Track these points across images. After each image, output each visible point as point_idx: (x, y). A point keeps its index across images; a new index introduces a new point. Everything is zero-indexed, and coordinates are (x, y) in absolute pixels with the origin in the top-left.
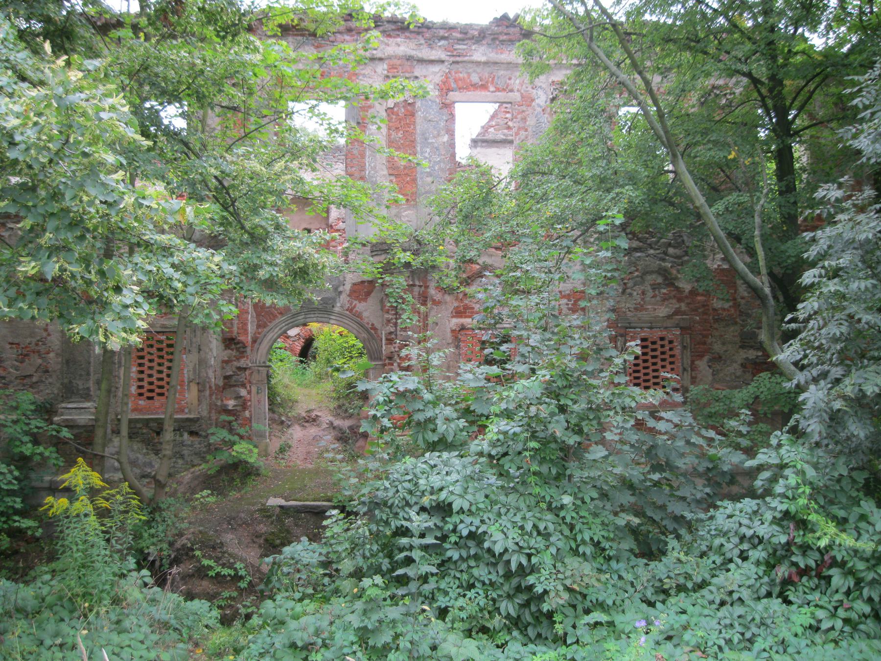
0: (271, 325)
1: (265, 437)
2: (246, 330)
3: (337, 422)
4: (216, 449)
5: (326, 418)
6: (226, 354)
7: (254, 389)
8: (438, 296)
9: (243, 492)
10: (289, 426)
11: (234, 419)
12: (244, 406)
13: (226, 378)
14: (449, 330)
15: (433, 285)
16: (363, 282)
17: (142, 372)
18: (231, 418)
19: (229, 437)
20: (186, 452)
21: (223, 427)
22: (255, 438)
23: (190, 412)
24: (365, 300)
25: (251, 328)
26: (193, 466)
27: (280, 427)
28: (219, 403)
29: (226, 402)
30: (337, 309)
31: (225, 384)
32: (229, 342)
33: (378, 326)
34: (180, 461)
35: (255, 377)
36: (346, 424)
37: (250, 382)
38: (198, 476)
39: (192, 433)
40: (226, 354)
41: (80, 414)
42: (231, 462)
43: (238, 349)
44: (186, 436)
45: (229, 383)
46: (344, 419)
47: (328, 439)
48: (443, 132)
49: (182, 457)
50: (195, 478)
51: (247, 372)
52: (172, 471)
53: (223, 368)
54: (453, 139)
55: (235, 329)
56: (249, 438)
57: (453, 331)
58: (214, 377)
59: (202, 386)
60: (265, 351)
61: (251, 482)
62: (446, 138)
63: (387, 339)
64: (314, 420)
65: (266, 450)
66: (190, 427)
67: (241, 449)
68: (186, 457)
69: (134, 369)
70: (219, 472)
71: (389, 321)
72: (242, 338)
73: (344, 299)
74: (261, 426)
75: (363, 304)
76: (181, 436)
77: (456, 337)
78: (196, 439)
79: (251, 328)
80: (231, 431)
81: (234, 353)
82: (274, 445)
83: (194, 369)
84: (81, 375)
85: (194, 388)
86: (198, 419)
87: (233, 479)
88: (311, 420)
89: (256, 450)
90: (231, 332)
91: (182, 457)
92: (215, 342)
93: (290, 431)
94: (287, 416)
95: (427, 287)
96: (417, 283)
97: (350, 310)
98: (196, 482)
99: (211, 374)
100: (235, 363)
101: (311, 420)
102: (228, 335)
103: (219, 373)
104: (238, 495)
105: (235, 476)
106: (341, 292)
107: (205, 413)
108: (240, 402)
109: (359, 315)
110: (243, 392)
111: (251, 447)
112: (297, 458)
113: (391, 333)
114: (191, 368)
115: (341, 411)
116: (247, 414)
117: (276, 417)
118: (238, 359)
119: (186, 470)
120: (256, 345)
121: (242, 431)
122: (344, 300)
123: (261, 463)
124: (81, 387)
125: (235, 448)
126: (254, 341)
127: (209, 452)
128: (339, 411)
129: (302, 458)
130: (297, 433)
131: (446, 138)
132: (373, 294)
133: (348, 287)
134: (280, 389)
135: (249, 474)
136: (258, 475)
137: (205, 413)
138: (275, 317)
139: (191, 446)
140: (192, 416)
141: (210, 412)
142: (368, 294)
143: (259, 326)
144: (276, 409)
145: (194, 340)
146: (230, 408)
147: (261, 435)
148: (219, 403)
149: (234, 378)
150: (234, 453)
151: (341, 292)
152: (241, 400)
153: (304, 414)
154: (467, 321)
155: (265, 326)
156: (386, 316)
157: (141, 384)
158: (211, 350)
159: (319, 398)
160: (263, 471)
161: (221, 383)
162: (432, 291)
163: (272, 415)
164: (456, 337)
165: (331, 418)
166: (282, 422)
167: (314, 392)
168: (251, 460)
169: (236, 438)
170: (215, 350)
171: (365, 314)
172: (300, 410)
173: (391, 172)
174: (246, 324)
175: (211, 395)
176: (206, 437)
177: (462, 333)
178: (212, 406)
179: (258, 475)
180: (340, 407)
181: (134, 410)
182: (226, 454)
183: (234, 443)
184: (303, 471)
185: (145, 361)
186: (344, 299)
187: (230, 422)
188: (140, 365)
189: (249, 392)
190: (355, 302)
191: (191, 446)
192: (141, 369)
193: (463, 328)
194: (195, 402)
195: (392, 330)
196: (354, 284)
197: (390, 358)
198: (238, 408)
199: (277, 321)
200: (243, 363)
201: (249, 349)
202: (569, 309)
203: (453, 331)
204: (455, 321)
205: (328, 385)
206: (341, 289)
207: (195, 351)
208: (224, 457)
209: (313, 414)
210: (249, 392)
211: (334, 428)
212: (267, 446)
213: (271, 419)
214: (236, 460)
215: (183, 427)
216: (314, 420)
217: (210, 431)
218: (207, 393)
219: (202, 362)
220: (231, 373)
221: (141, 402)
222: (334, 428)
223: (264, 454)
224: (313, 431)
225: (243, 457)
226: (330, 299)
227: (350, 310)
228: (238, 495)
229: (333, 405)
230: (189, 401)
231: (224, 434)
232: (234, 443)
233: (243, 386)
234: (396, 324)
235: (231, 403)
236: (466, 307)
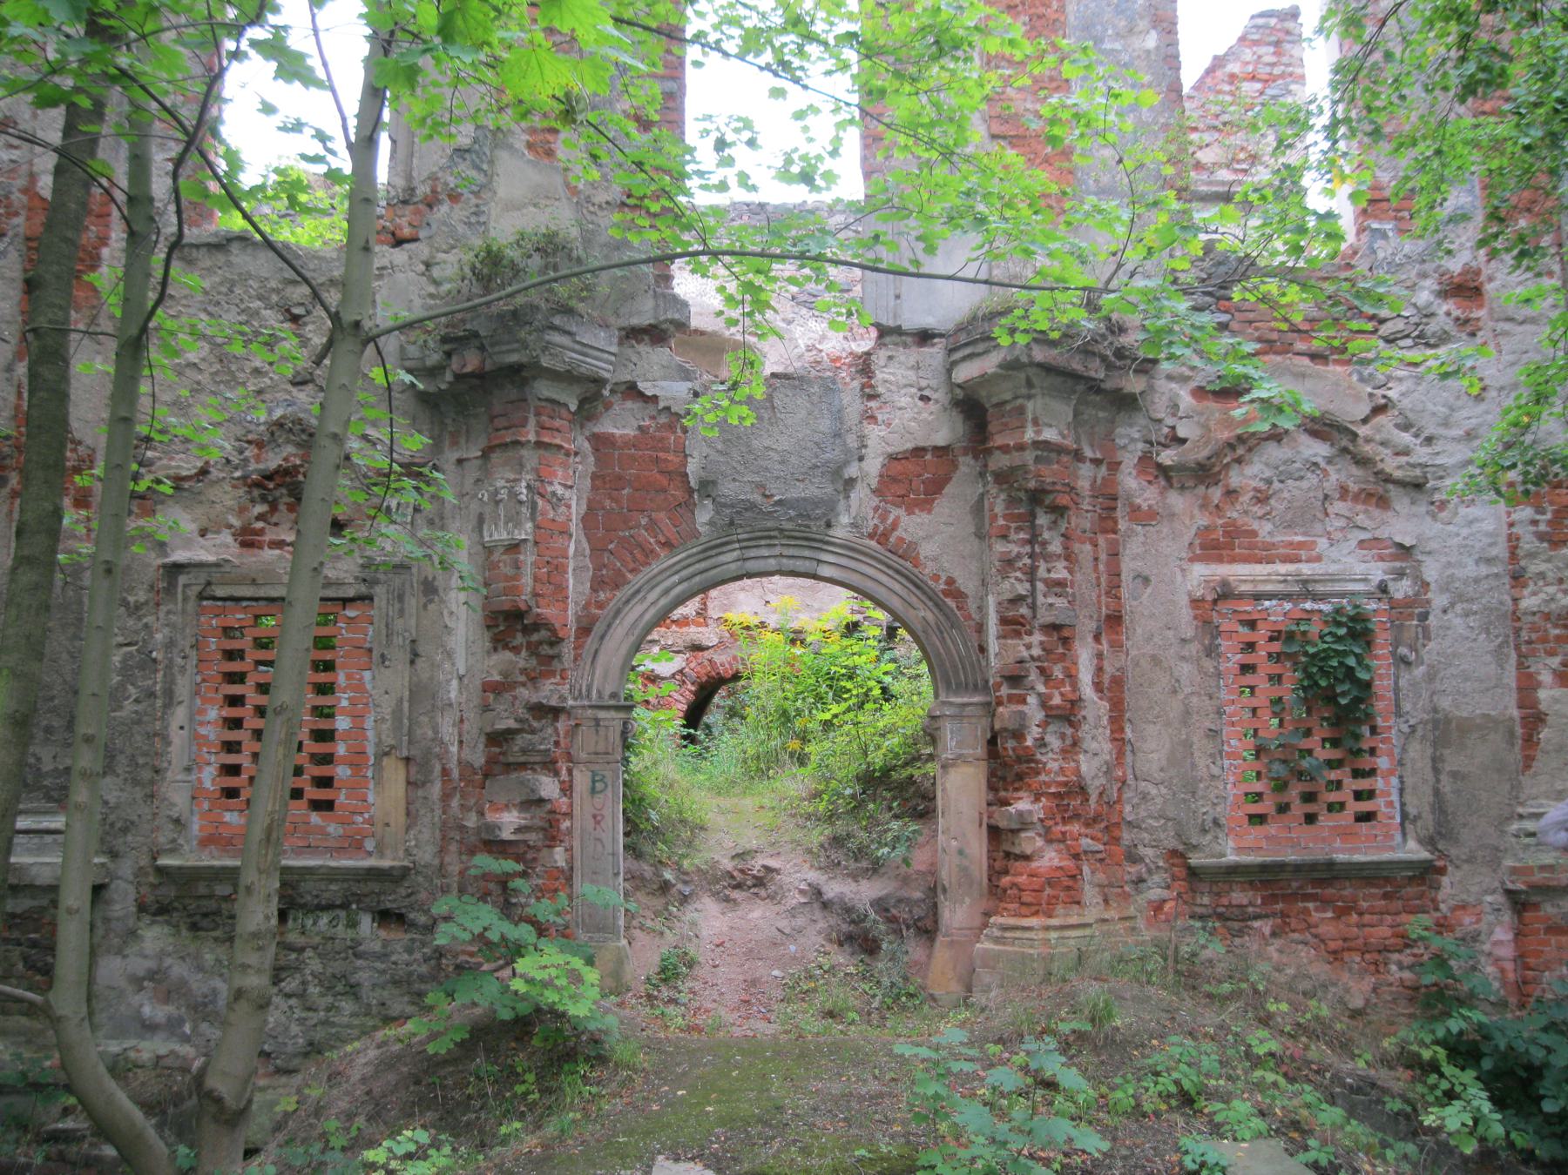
0: (637, 580)
1: (614, 930)
2: (561, 589)
3: (834, 888)
4: (459, 968)
5: (797, 874)
6: (496, 665)
7: (581, 779)
8: (1145, 494)
9: (551, 1130)
10: (684, 899)
11: (516, 871)
12: (551, 833)
13: (497, 739)
14: (1184, 601)
15: (1129, 460)
16: (918, 451)
17: (236, 723)
18: (510, 866)
19: (500, 928)
20: (364, 977)
21: (483, 898)
22: (582, 936)
23: (380, 851)
24: (926, 504)
25: (576, 586)
26: (388, 1020)
27: (658, 903)
28: (471, 821)
29: (491, 817)
30: (840, 532)
31: (491, 761)
32: (509, 624)
33: (968, 585)
34: (347, 1006)
35: (585, 743)
36: (863, 893)
37: (569, 757)
38: (399, 1057)
39: (385, 917)
40: (496, 665)
41: (40, 850)
42: (506, 1015)
43: (533, 649)
44: (366, 923)
45: (503, 755)
46: (855, 877)
47: (813, 940)
48: (1143, 24)
49: (353, 990)
50: (387, 1064)
51: (562, 725)
52: (319, 1035)
53: (486, 708)
54: (1174, 44)
55: (527, 581)
56: (565, 933)
57: (1196, 603)
58: (456, 737)
59: (417, 767)
60: (617, 662)
61: (575, 1086)
62: (1151, 41)
63: (1004, 621)
64: (760, 882)
65: (617, 974)
66: (386, 898)
67: (543, 971)
68: (365, 992)
69: (213, 714)
70: (466, 1048)
71: (1009, 562)
72: (548, 611)
73: (861, 501)
74: (604, 892)
75: (921, 517)
76: (353, 924)
77: (1207, 623)
78: (398, 937)
79: (576, 586)
80: (508, 909)
81: (522, 660)
82: (644, 957)
83: (397, 712)
84: (49, 730)
85: (396, 776)
86: (405, 873)
87: (513, 1076)
88: (748, 882)
89: (592, 975)
90: (515, 590)
91: (353, 990)
92: (462, 611)
93: (689, 914)
94: (680, 870)
95: (1115, 466)
96: (1088, 453)
97: (882, 537)
98: (392, 1077)
99: (448, 731)
100: (524, 693)
101: (748, 882)
102: (505, 603)
103: (473, 726)
104: (531, 1142)
105: (520, 1061)
106: (850, 483)
107: (426, 855)
108: (538, 817)
109: (907, 552)
110: (548, 787)
111: (577, 963)
112: (717, 997)
113: (1017, 600)
114: (387, 711)
115: (844, 852)
116: (559, 856)
117: (647, 870)
118: (533, 679)
119: (365, 1032)
120: (590, 642)
121: (544, 910)
122: (858, 509)
123: (611, 1021)
124: (47, 766)
125: (522, 965)
126: (584, 630)
127: (434, 977)
128: (835, 855)
129: (733, 998)
130: (709, 920)
131: (1151, 41)
132: (948, 489)
133: (873, 465)
134: (652, 789)
135: (570, 1056)
136: (602, 1060)
137: (426, 855)
138: (649, 554)
139: (382, 957)
140: (386, 863)
141: (442, 851)
142: (936, 487)
143: (598, 584)
144: (647, 848)
145: (399, 624)
146: (506, 835)
147: (602, 926)
148: (471, 821)
149: (521, 741)
150: (518, 985)
151: (850, 483)
152: (540, 813)
153: (727, 864)
154: (1241, 573)
155: (617, 583)
156: (1000, 547)
157: (232, 759)
158: (449, 655)
159: (766, 818)
160: (621, 1052)
161: (478, 758)
162: (1130, 481)
163: (635, 865)
164: (1207, 623)
165: (813, 876)
166: (665, 887)
167: (749, 803)
168: (578, 1010)
169: (525, 932)
170: (461, 645)
171: (926, 550)
172: (717, 851)
173: (997, 128)
174: (560, 569)
175: (446, 797)
176: (430, 928)
177: (1224, 607)
178: (449, 832)
179: (602, 1060)
180: (837, 841)
181: (205, 842)
182: (491, 988)
183: (516, 950)
184: (752, 1048)
185: (247, 690)
186: (861, 501)
187: (503, 881)
188: (235, 701)
189: (567, 789)
190: (896, 512)
191: (382, 957)
192: (235, 712)
193: (1225, 593)
194: (398, 818)
195: (1023, 589)
196: (893, 458)
197: (1015, 679)
198: (532, 837)
199: (655, 567)
200: (548, 692)
201: (567, 650)
202: (1541, 537)
203: (1196, 603)
204: (1200, 571)
205: (793, 783)
206: (852, 471)
207: (399, 657)
208: (483, 996)
209: (757, 864)
210: (567, 789)
211: (826, 905)
212: (620, 961)
213: (631, 877)
214: (524, 1008)
215: (359, 898)
216: (760, 882)
217: (440, 907)
218: (436, 790)
219: (422, 695)
220: (512, 724)
221: (229, 817)
222: (826, 905)
223: (615, 986)
224: (758, 915)
225: (551, 996)
226: (816, 503)
227: (882, 537)
228: (531, 1142)
229: (818, 836)
230: (384, 815)
231: (484, 917)
232: (517, 950)
233: (550, 766)
234: (1031, 574)
235: (509, 821)
236: (1234, 532)
